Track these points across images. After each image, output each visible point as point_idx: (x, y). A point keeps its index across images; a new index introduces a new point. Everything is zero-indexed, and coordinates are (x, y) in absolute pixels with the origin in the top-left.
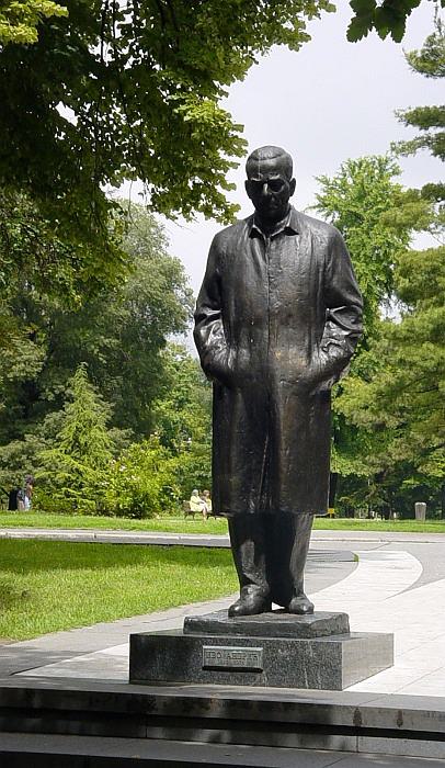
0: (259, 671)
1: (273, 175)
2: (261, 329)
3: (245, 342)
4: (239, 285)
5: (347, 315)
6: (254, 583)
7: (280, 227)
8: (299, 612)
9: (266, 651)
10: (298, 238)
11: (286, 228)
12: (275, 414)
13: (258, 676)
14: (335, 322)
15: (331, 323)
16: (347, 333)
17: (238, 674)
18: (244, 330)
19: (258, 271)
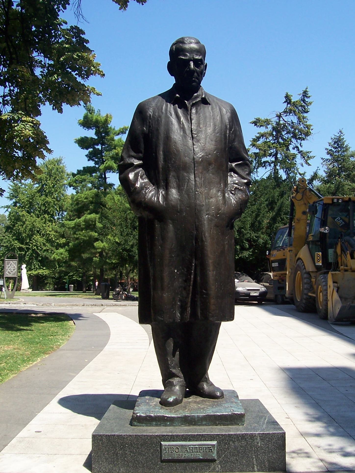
0: (213, 461)
1: (197, 55)
2: (187, 172)
3: (173, 182)
4: (168, 138)
5: (239, 167)
6: (178, 377)
7: (197, 97)
8: (212, 396)
9: (219, 443)
10: (210, 107)
11: (202, 98)
12: (202, 241)
13: (212, 465)
14: (235, 172)
15: (232, 174)
16: (246, 181)
17: (195, 465)
18: (172, 174)
19: (182, 128)
